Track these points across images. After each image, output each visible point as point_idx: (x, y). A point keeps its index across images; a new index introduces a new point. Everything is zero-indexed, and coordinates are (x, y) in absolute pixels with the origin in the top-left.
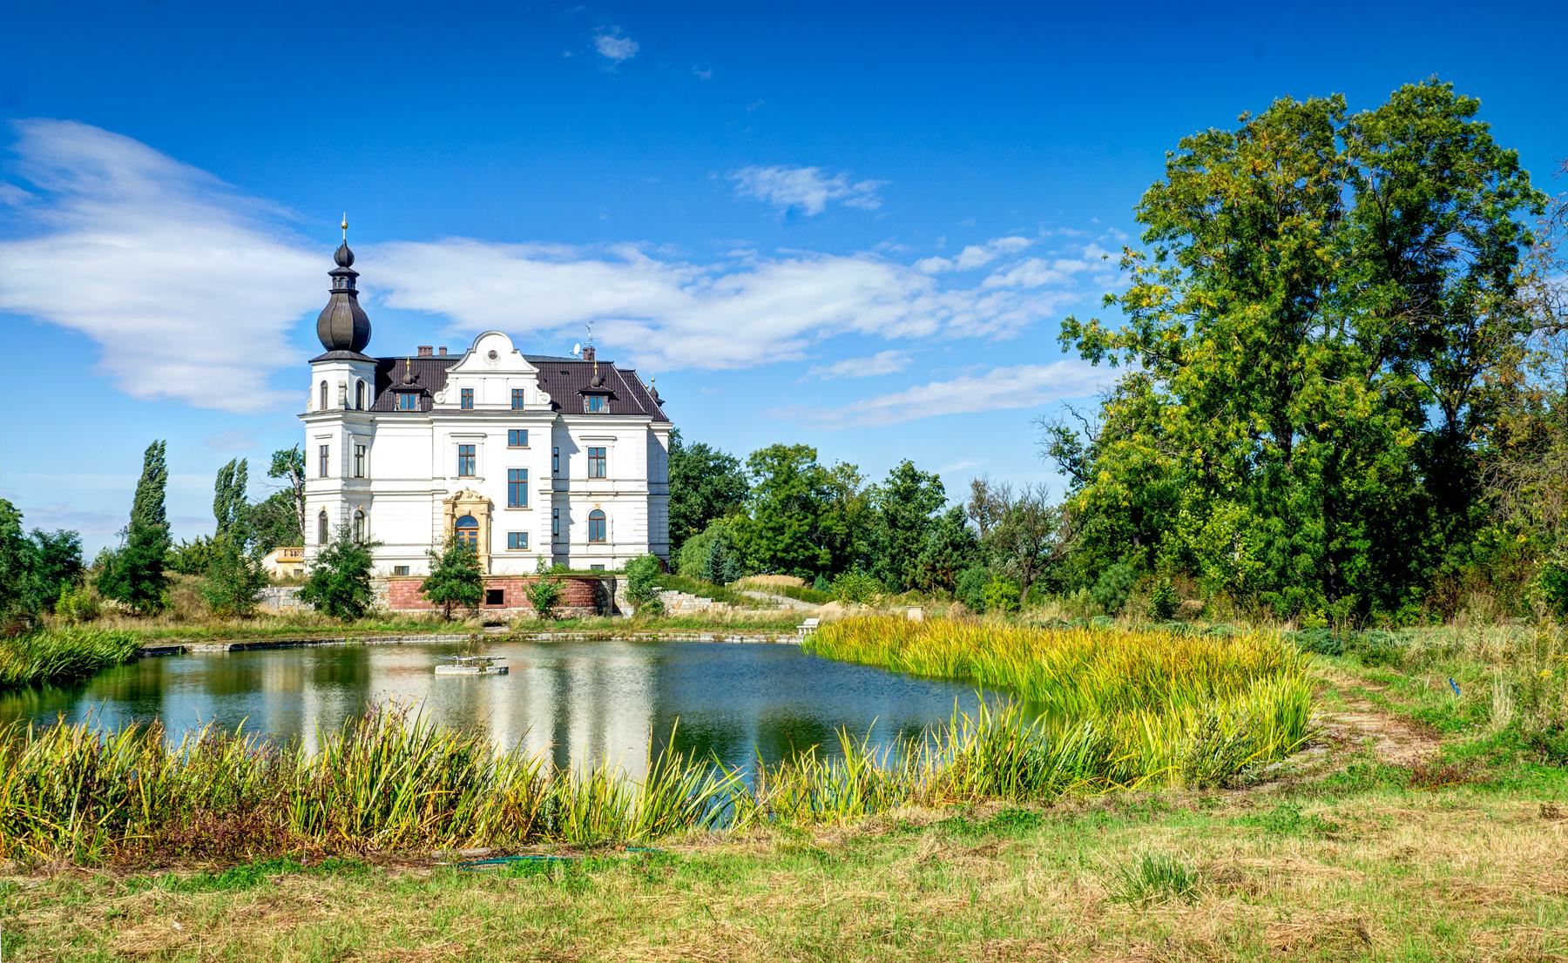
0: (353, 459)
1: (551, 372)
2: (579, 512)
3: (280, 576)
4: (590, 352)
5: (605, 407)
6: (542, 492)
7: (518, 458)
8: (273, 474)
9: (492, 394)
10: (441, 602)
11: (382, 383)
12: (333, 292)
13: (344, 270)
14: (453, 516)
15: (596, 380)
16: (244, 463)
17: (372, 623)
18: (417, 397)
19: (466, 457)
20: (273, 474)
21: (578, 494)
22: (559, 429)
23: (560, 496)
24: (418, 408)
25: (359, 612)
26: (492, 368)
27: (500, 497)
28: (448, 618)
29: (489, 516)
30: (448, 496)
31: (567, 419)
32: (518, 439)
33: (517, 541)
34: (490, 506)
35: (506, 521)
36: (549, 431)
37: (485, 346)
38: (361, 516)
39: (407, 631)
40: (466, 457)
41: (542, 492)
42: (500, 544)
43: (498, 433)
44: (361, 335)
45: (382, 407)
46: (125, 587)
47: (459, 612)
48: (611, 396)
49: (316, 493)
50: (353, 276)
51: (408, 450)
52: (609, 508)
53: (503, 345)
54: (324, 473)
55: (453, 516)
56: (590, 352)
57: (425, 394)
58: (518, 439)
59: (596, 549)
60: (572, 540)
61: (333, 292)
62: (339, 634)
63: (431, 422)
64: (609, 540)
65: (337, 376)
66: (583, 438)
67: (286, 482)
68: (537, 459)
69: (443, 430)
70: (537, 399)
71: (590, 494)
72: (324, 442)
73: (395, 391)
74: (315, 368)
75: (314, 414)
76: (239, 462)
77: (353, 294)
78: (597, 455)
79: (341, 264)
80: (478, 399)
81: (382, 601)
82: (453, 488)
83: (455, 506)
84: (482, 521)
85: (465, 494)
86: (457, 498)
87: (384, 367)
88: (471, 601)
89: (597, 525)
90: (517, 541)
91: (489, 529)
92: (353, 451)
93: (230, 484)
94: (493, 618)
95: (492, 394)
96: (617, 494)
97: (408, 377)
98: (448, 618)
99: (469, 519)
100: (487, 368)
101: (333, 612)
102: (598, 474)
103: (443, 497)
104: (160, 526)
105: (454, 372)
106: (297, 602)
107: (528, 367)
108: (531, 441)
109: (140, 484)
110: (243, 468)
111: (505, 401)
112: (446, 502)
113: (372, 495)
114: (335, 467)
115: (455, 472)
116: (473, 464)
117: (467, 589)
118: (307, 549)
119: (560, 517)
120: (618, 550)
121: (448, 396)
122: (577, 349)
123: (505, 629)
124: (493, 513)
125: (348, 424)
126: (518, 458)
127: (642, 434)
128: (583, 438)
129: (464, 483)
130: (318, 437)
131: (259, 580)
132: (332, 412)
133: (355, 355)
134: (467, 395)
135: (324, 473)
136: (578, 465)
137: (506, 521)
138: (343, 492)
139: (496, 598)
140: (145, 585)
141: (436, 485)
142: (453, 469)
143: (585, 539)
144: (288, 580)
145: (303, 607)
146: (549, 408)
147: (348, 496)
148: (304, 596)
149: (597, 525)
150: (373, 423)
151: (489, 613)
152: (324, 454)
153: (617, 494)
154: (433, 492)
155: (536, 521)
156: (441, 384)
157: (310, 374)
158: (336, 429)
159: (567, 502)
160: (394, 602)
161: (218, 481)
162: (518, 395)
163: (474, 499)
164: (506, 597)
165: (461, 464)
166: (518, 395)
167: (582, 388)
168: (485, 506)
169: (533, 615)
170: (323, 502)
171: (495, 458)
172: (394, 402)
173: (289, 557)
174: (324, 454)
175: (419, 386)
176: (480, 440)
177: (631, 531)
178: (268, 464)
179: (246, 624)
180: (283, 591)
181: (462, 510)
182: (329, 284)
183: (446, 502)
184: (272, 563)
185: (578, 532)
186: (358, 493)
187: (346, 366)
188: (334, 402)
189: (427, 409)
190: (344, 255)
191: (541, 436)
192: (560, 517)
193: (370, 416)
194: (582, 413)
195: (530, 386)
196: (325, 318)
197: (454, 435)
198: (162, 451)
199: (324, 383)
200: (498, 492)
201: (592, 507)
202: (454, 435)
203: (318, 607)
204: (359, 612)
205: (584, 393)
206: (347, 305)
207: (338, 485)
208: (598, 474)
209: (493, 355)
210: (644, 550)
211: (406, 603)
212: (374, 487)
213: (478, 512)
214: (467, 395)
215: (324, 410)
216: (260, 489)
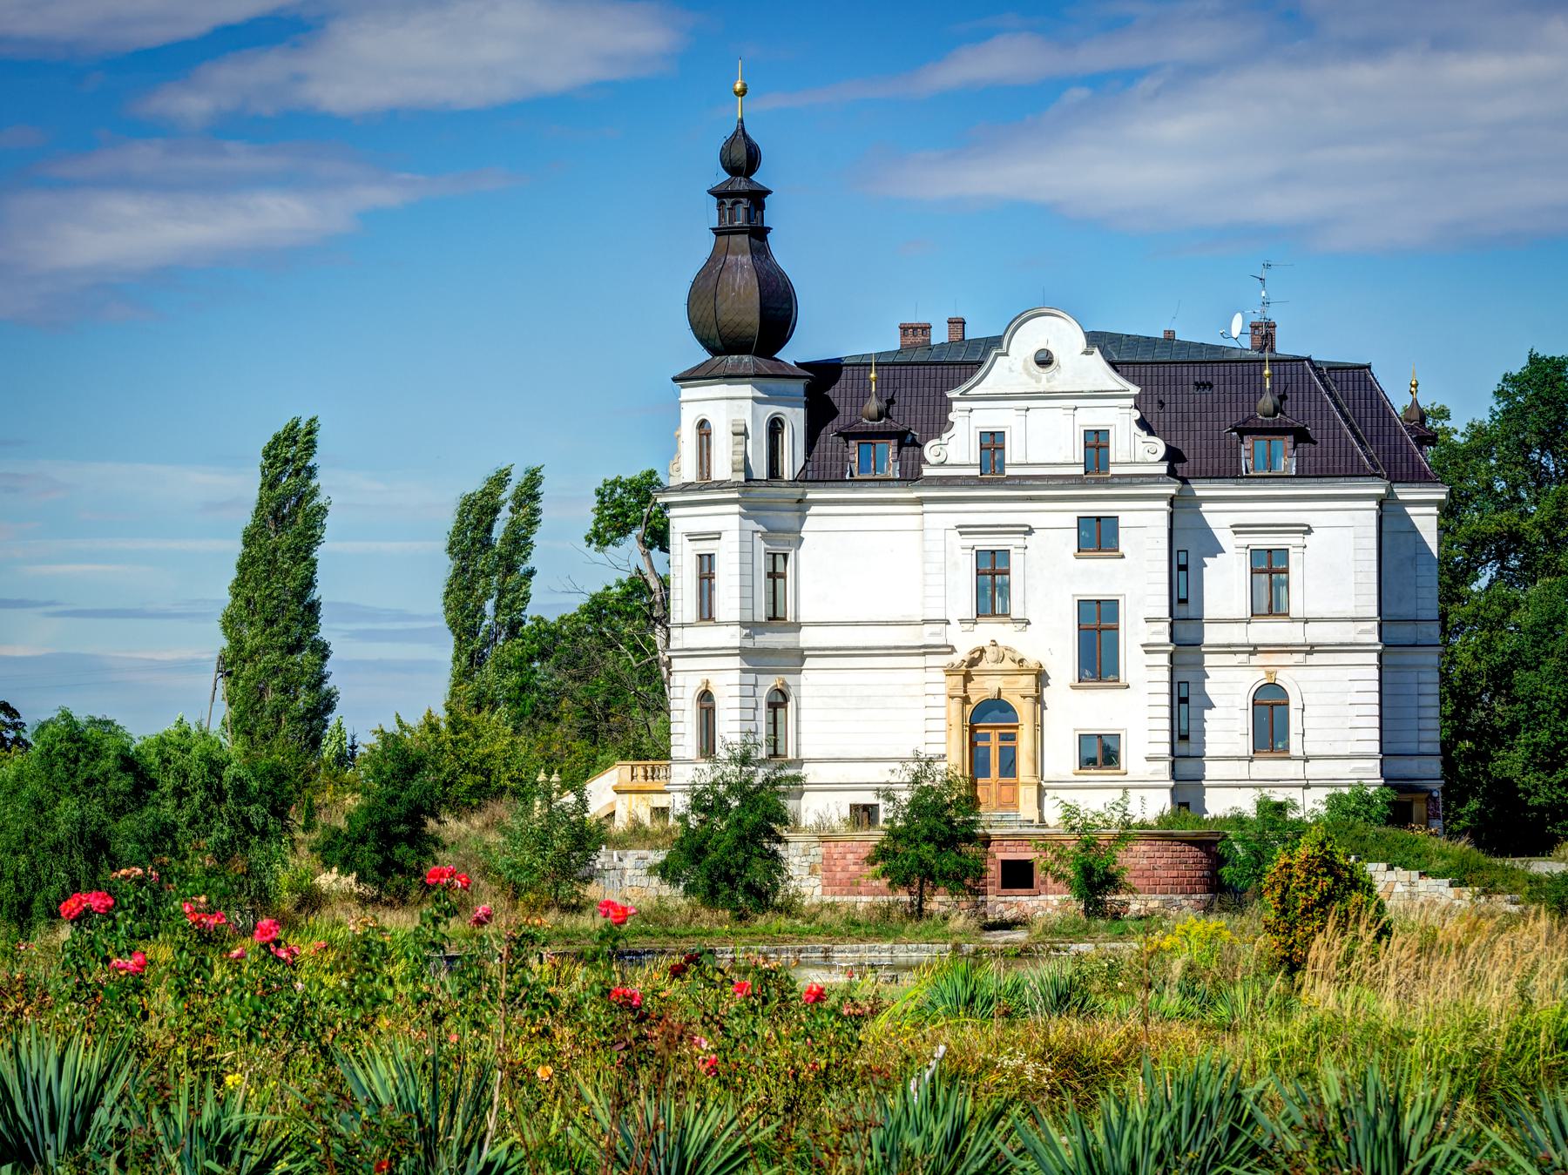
0: (762, 582)
1: (1164, 377)
2: (1229, 692)
3: (620, 824)
4: (1264, 334)
5: (1287, 463)
6: (1149, 648)
7: (1096, 578)
8: (598, 538)
9: (1045, 440)
10: (906, 883)
11: (819, 414)
12: (718, 232)
13: (741, 185)
14: (966, 700)
15: (1267, 402)
16: (533, 479)
17: (783, 922)
18: (891, 448)
19: (992, 575)
20: (598, 538)
21: (1229, 649)
22: (1182, 512)
23: (1187, 655)
24: (893, 471)
25: (762, 898)
26: (1042, 387)
27: (1062, 660)
28: (918, 913)
29: (1039, 700)
30: (956, 659)
31: (1201, 489)
32: (1098, 537)
33: (1101, 753)
34: (1041, 677)
35: (1074, 711)
36: (1162, 520)
37: (1027, 341)
38: (779, 702)
39: (844, 936)
40: (992, 575)
41: (1149, 648)
42: (1062, 758)
43: (1056, 523)
44: (778, 313)
45: (819, 473)
46: (367, 854)
47: (938, 902)
48: (1301, 436)
49: (692, 653)
50: (757, 198)
51: (873, 560)
52: (1294, 679)
53: (1061, 334)
54: (706, 614)
55: (966, 700)
56: (1264, 334)
57: (908, 442)
58: (1098, 537)
59: (1267, 768)
60: (1210, 751)
61: (718, 232)
62: (725, 941)
63: (921, 501)
64: (1295, 748)
65: (729, 411)
66: (1239, 529)
67: (628, 554)
68: (1137, 580)
69: (942, 520)
70: (1137, 450)
71: (1255, 650)
72: (705, 547)
73: (847, 436)
74: (686, 393)
75: (685, 488)
76: (517, 478)
77: (759, 234)
78: (1270, 568)
79: (732, 169)
80: (1014, 453)
81: (804, 873)
82: (965, 641)
83: (968, 678)
84: (1024, 710)
85: (990, 655)
86: (973, 662)
87: (822, 378)
88: (967, 881)
89: (1270, 719)
90: (1101, 753)
91: (1039, 727)
92: (762, 565)
93: (489, 544)
94: (1009, 915)
95: (1045, 440)
96: (1312, 649)
97: (873, 406)
98: (918, 913)
99: (996, 708)
100: (1033, 387)
101: (711, 897)
102: (1270, 604)
103: (944, 660)
104: (305, 657)
105: (965, 397)
106: (655, 880)
107: (1111, 381)
108: (1125, 540)
109: (249, 539)
110: (529, 494)
111: (1067, 453)
112: (950, 671)
113: (798, 657)
114: (728, 602)
115: (967, 607)
116: (1005, 590)
117: (949, 862)
118: (675, 768)
119: (1186, 700)
120: (1315, 770)
121: (954, 449)
122: (1237, 325)
123: (1019, 936)
124: (1048, 694)
125: (751, 510)
126: (1096, 578)
127: (1365, 518)
128: (1239, 529)
129: (987, 632)
130: (694, 537)
131: (587, 839)
132: (721, 485)
133: (764, 365)
134: (992, 443)
135: (706, 614)
136: (1225, 585)
137: (1074, 711)
138: (743, 652)
139: (1018, 875)
140: (401, 851)
141: (927, 635)
142: (965, 602)
143: (1245, 745)
144: (638, 835)
145: (666, 890)
146: (1163, 469)
147: (754, 659)
148: (665, 871)
149: (1270, 719)
150: (802, 504)
151: (1003, 904)
152: (706, 569)
153: (1312, 649)
154: (926, 650)
155: (1136, 710)
156: (940, 425)
157: (676, 407)
158: (727, 521)
159: (1199, 665)
160: (830, 882)
161: (459, 531)
162: (1096, 443)
163: (1008, 665)
164: (1039, 874)
165: (980, 590)
166: (1096, 443)
167: (1236, 418)
168: (1028, 682)
169: (1076, 907)
170: (702, 664)
171: (1052, 578)
172: (845, 460)
173: (640, 782)
174: (706, 569)
175: (895, 425)
176: (1017, 540)
177: (1341, 731)
178: (586, 516)
179: (568, 921)
180: (631, 859)
181: (984, 688)
182: (711, 215)
183: (950, 671)
184: (609, 794)
185: (1227, 728)
186: (773, 649)
187: (746, 390)
188: (722, 469)
189: (912, 476)
190: (740, 154)
191: (1145, 527)
192: (1186, 700)
193: (796, 492)
194: (1232, 474)
195: (1120, 420)
196: (704, 294)
197: (964, 530)
198: (310, 446)
199: (703, 424)
200: (1052, 642)
201: (1260, 677)
202: (964, 530)
203: (690, 889)
204: (762, 898)
205: (1243, 432)
206: (745, 259)
207: (731, 637)
208: (1270, 604)
209: (1044, 360)
210: (1369, 773)
211: (852, 886)
212: (807, 638)
213: (1016, 692)
214: (992, 443)
215: (705, 482)
216: (567, 573)
